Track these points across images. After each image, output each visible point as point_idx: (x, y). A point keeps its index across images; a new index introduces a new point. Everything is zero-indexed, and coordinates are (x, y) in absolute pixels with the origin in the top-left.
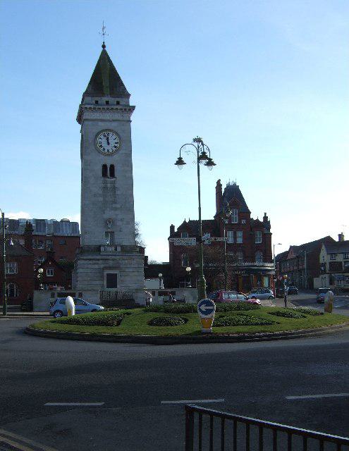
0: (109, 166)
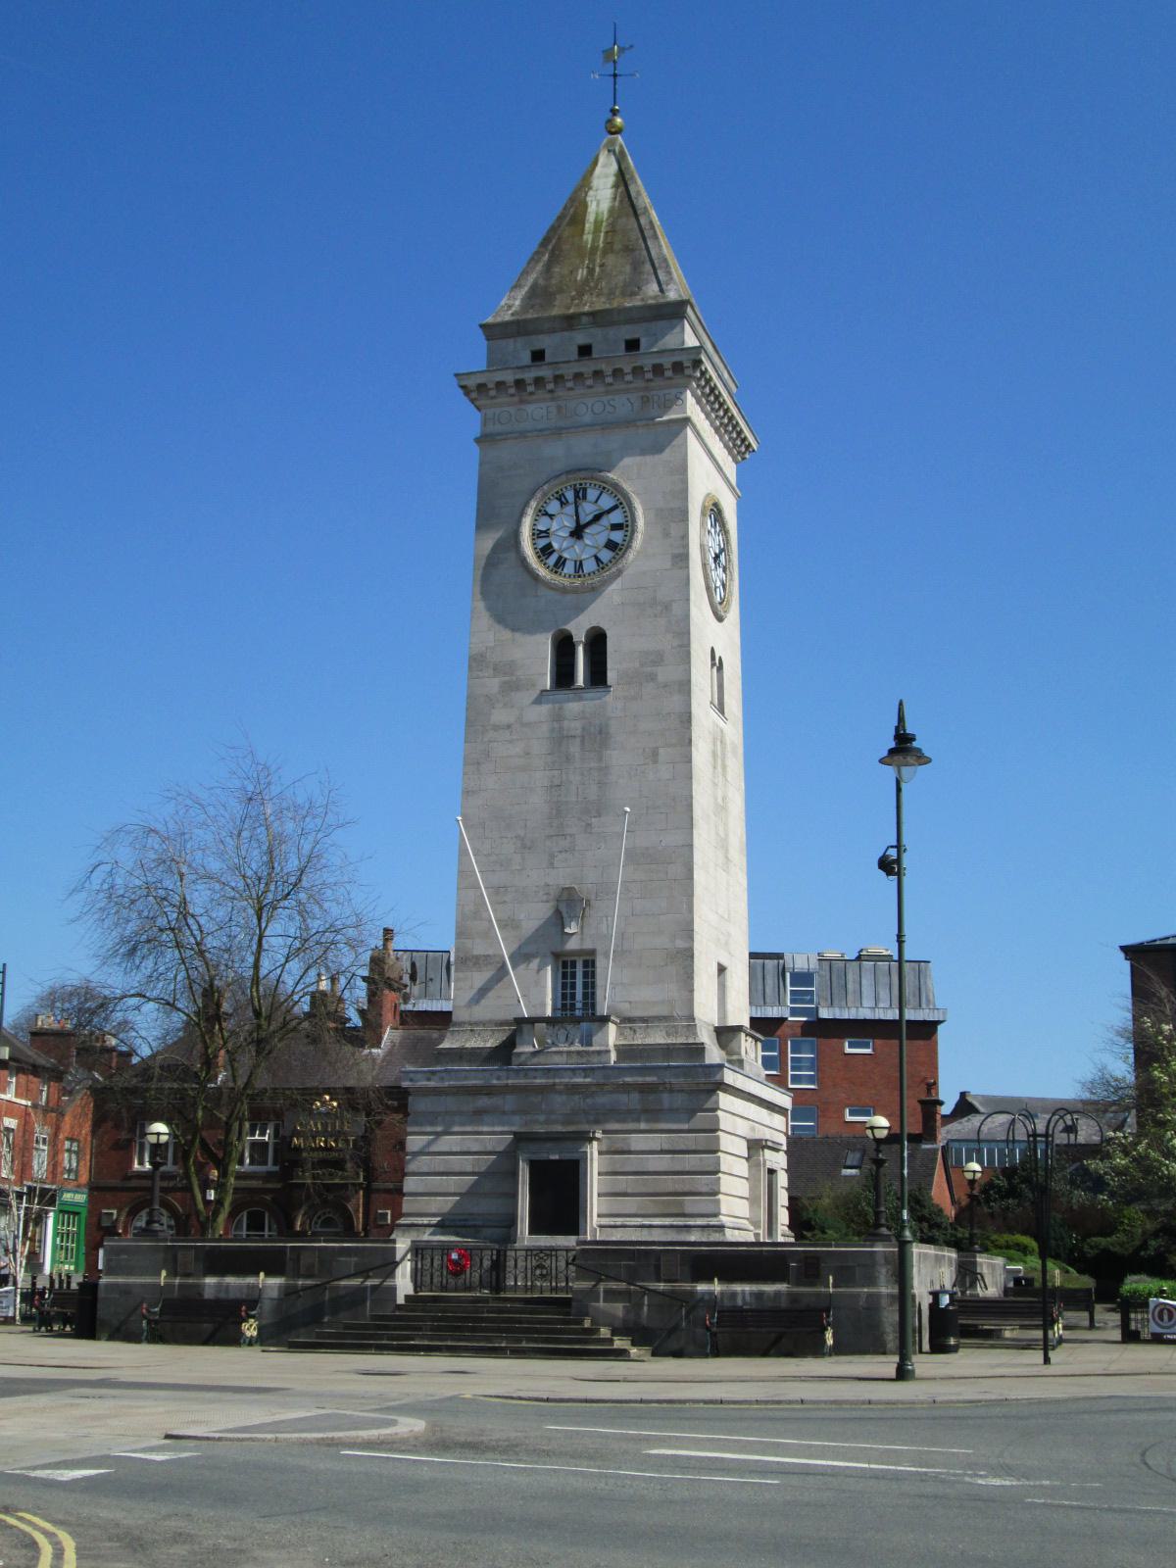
0: (580, 637)
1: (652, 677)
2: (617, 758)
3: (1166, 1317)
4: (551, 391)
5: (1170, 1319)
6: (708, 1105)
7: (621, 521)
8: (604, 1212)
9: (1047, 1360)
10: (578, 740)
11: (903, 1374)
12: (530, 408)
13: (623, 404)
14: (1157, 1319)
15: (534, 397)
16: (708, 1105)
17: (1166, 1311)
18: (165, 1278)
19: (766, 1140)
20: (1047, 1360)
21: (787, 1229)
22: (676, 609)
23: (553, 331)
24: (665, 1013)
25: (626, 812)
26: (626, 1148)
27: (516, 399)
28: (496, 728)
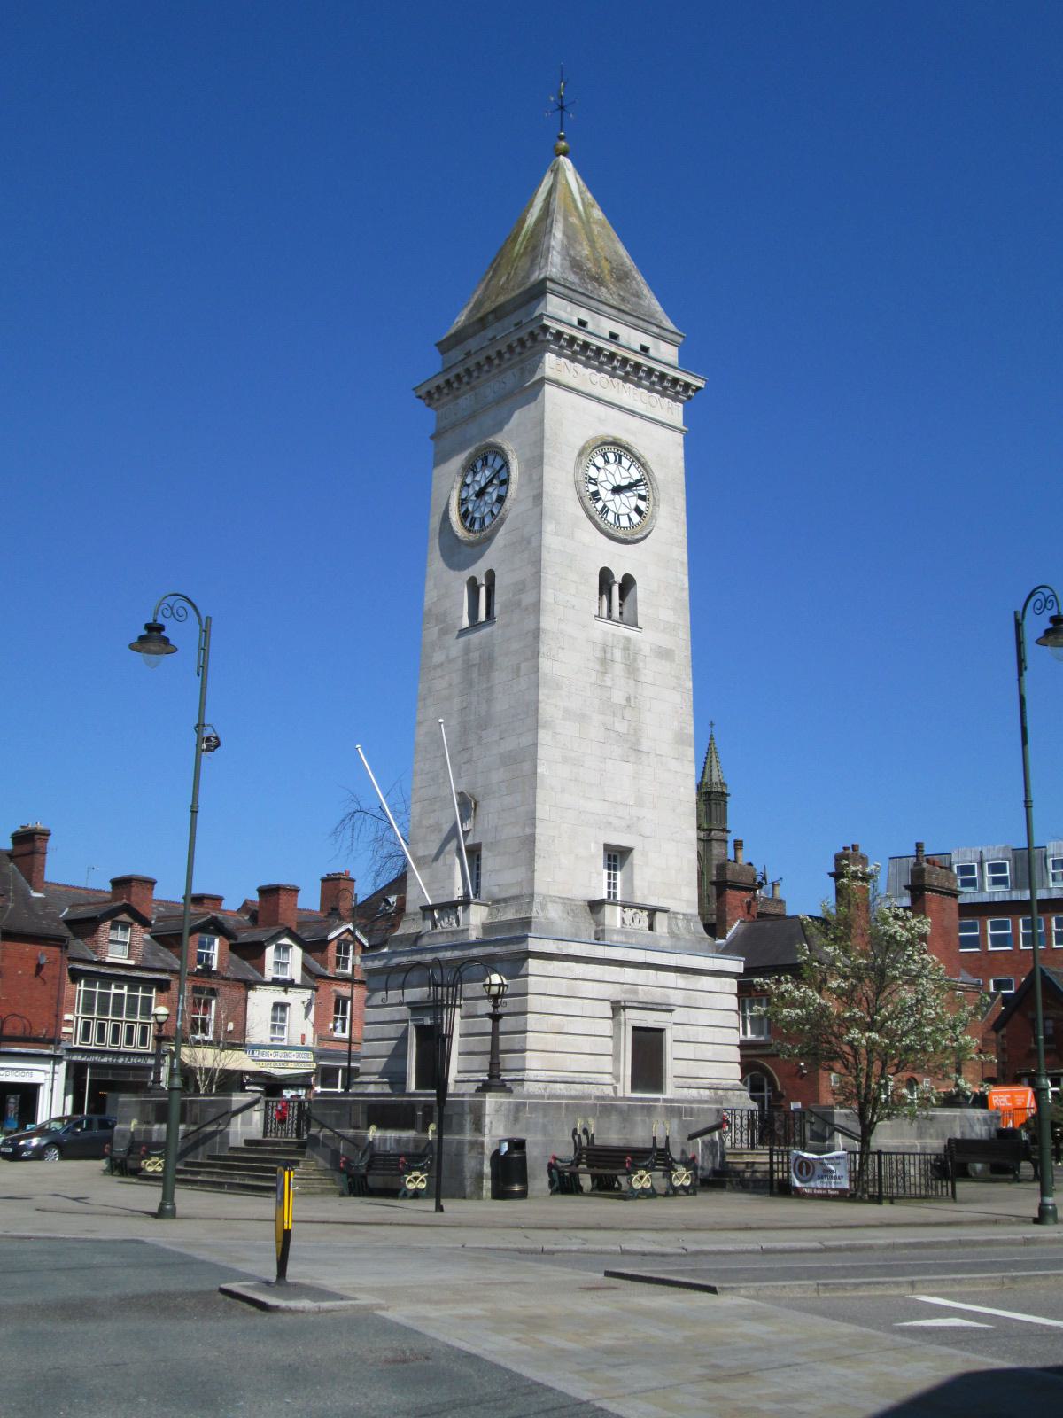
1: (519, 604)
2: (499, 677)
3: (804, 1171)
4: (468, 383)
5: (808, 1172)
6: (522, 972)
7: (640, 477)
8: (461, 1069)
9: (439, 1208)
10: (477, 667)
11: (164, 1212)
12: (460, 401)
13: (510, 379)
14: (797, 1171)
15: (461, 391)
16: (522, 972)
17: (804, 1164)
18: (135, 1125)
19: (625, 1002)
20: (439, 1208)
21: (738, 1082)
22: (534, 544)
23: (475, 334)
24: (518, 893)
25: (441, 723)
26: (474, 1014)
27: (450, 397)
28: (436, 667)
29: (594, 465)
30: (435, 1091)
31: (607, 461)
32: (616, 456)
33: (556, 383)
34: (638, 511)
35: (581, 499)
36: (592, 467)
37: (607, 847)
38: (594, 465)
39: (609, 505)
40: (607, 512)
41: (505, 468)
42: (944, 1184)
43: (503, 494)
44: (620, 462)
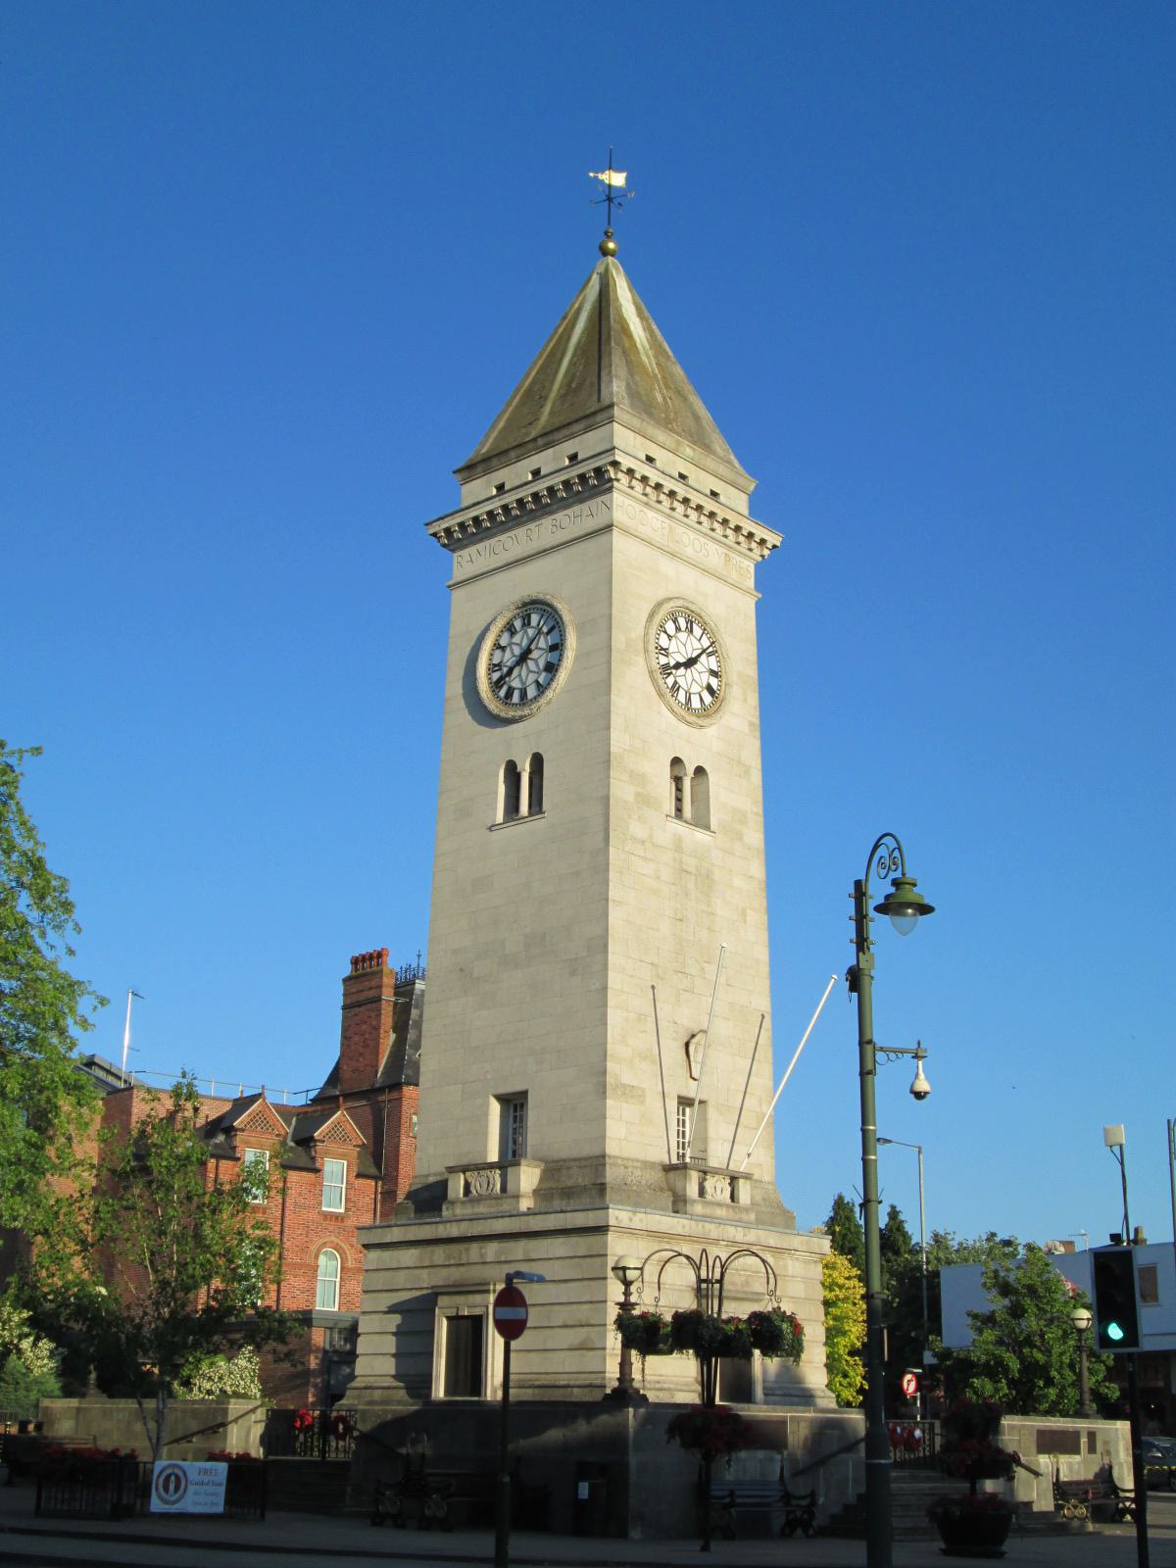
3: (172, 1487)
5: (177, 1489)
17: (173, 1478)
29: (665, 632)
30: (714, 1359)
31: (678, 629)
32: (687, 623)
33: (626, 531)
34: (709, 688)
35: (651, 673)
36: (663, 634)
37: (524, 1094)
38: (665, 632)
39: (681, 681)
40: (678, 689)
41: (557, 630)
42: (252, 1511)
43: (555, 662)
44: (691, 631)
